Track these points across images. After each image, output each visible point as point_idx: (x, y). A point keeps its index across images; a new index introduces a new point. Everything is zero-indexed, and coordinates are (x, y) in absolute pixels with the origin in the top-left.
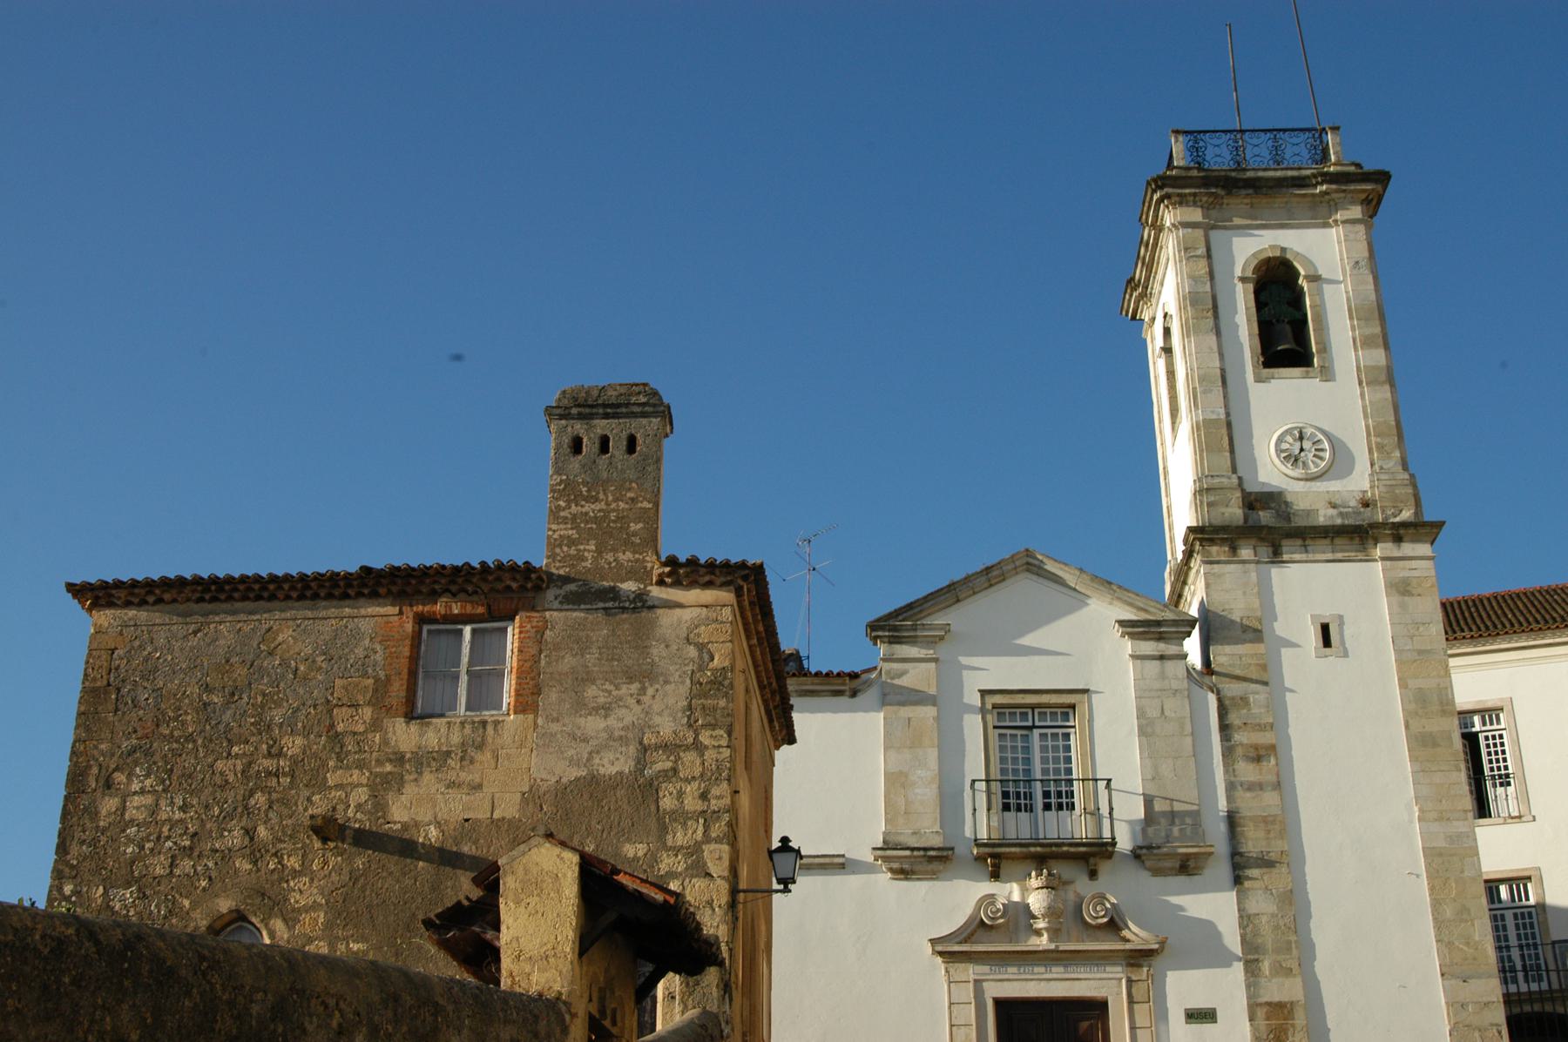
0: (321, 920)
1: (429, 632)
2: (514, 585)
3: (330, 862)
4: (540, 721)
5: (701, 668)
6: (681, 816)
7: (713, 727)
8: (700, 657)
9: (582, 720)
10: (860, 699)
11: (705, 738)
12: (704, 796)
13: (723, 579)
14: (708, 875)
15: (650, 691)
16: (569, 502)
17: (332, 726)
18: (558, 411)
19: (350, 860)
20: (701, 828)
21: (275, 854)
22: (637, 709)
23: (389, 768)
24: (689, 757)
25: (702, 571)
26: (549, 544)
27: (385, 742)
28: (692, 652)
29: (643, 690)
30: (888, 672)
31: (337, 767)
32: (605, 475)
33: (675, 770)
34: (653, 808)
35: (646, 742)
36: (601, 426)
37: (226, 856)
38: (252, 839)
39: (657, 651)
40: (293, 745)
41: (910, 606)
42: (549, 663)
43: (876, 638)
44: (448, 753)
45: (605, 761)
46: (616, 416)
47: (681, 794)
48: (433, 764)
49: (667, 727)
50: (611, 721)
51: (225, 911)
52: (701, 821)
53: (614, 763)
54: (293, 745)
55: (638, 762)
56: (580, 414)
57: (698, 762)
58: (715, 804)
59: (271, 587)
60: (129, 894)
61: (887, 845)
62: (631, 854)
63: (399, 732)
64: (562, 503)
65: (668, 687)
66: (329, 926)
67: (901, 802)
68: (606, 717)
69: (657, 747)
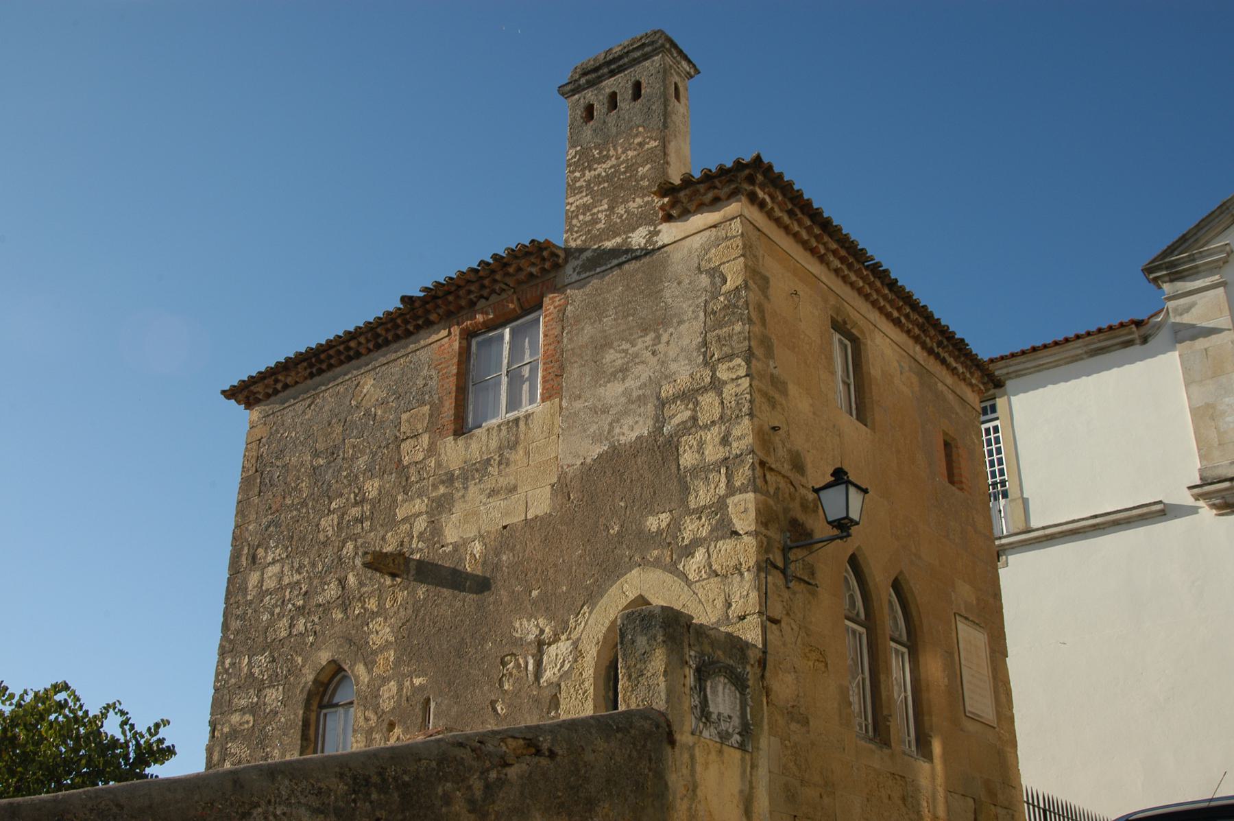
0: (392, 659)
1: (478, 343)
2: (534, 270)
3: (401, 595)
4: (564, 404)
5: (714, 297)
6: (702, 470)
7: (729, 357)
8: (713, 284)
9: (602, 390)
10: (1152, 343)
11: (723, 374)
12: (725, 441)
13: (727, 190)
14: (736, 533)
15: (665, 338)
16: (583, 170)
17: (400, 461)
18: (568, 88)
19: (413, 593)
20: (723, 479)
21: (359, 599)
22: (653, 361)
23: (442, 490)
24: (708, 401)
25: (702, 188)
26: (567, 218)
27: (439, 465)
28: (704, 280)
29: (658, 338)
30: (1175, 310)
31: (404, 501)
32: (614, 130)
33: (694, 419)
34: (674, 466)
35: (663, 395)
36: (609, 85)
37: (326, 608)
38: (343, 588)
39: (670, 292)
40: (372, 488)
41: (1183, 239)
42: (570, 340)
43: (1155, 280)
44: (489, 460)
45: (625, 427)
46: (621, 69)
47: (701, 444)
48: (477, 476)
49: (684, 373)
50: (630, 383)
51: (324, 663)
52: (723, 470)
53: (634, 429)
54: (372, 488)
55: (657, 421)
56: (588, 82)
57: (717, 401)
58: (737, 447)
59: (353, 344)
60: (262, 659)
61: (1205, 482)
62: (654, 529)
63: (449, 451)
64: (577, 174)
65: (683, 327)
66: (398, 662)
67: (1213, 435)
68: (623, 380)
69: (675, 398)
